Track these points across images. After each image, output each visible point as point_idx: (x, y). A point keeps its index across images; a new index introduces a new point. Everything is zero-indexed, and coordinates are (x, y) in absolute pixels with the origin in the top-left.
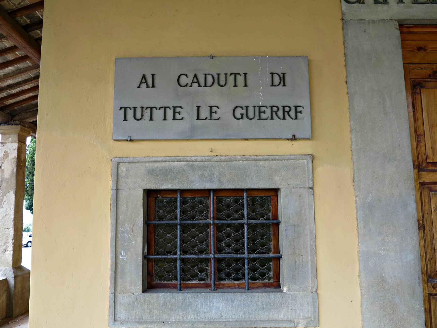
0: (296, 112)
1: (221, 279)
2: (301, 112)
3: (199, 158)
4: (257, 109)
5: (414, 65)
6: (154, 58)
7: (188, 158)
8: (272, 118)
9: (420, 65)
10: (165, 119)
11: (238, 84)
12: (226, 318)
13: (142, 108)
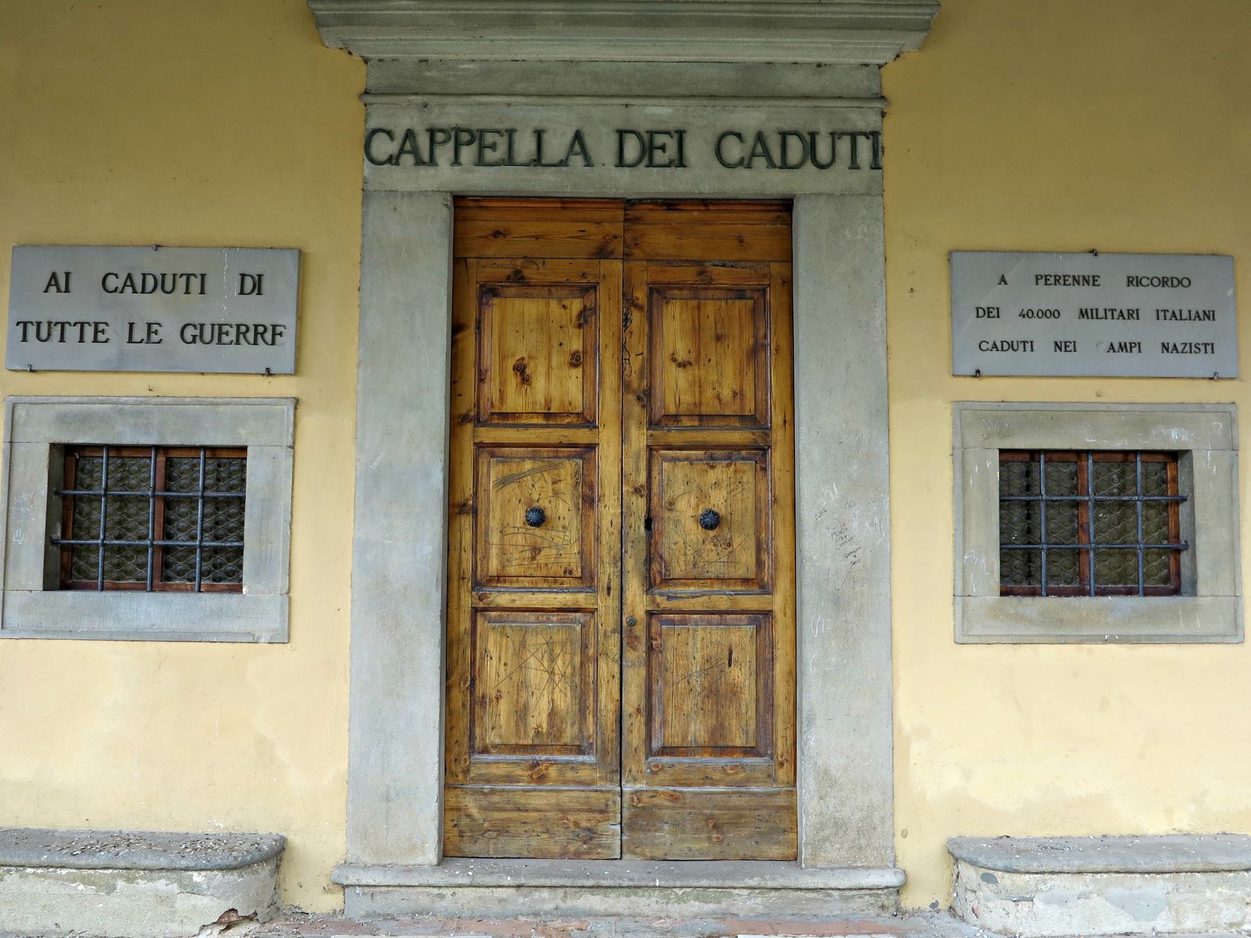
0: (274, 334)
1: (169, 578)
2: (281, 334)
3: (131, 400)
4: (216, 328)
5: (486, 260)
6: (71, 246)
7: (115, 399)
8: (238, 343)
9: (495, 261)
10: (81, 340)
11: (191, 290)
12: (158, 628)
13: (49, 323)
